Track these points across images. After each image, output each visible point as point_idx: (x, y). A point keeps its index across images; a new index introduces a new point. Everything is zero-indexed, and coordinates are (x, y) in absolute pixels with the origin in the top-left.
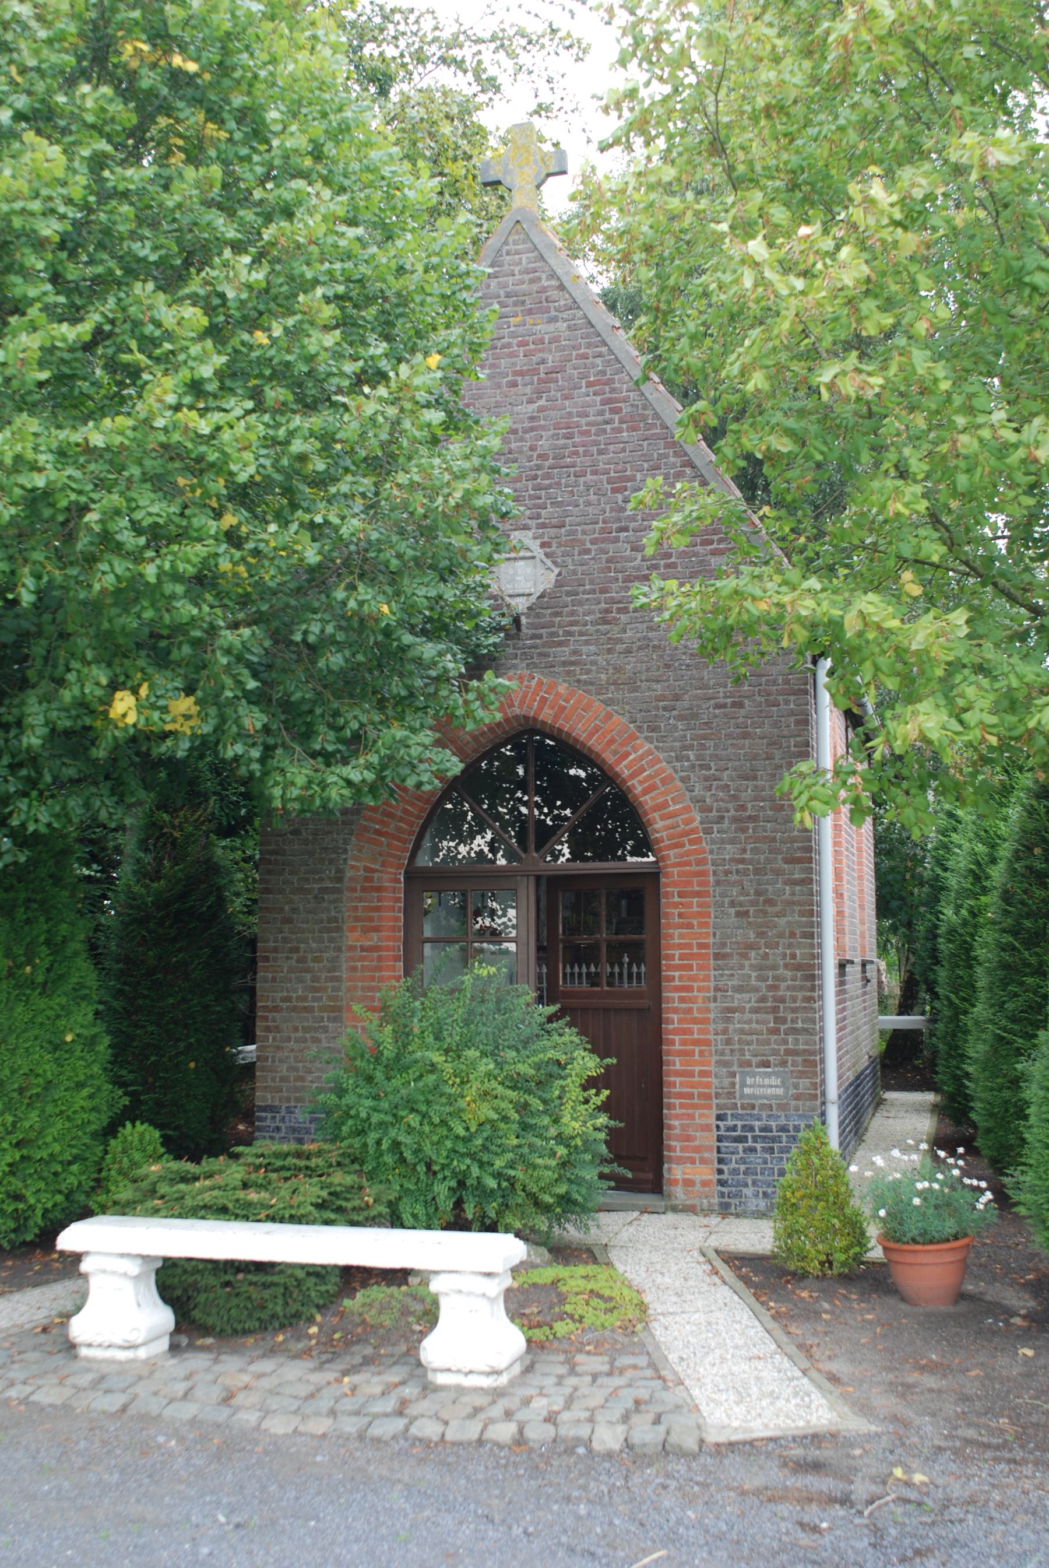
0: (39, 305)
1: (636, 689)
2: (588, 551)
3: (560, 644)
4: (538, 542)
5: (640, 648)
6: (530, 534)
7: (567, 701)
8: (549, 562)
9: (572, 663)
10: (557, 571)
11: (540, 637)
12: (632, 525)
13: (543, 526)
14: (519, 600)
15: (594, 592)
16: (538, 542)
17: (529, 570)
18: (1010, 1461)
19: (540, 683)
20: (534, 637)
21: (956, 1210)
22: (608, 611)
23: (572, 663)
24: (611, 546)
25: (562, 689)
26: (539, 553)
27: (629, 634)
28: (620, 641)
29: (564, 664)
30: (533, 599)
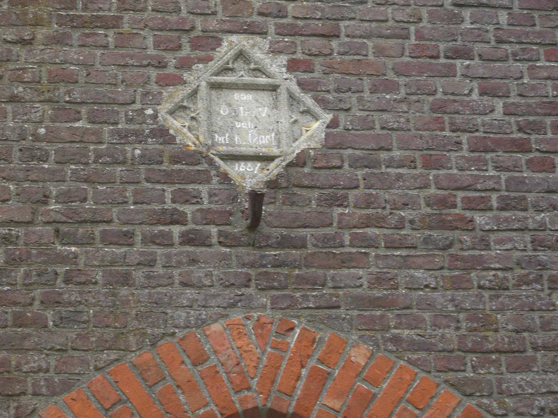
0: (448, 205)
1: (526, 366)
2: (392, 87)
3: (346, 262)
4: (283, 59)
5: (523, 281)
6: (265, 43)
7: (374, 382)
8: (308, 100)
9: (375, 303)
10: (328, 117)
11: (301, 244)
12: (478, 48)
13: (293, 31)
14: (242, 167)
15: (412, 164)
16: (283, 59)
17: (264, 112)
18: (41, 245)
19: (308, 342)
20: (284, 243)
21: (269, 395)
22: (444, 203)
23: (375, 303)
24: (439, 83)
25: (359, 355)
26: (289, 83)
27: (496, 251)
28: (477, 263)
29: (362, 303)
30: (274, 169)
